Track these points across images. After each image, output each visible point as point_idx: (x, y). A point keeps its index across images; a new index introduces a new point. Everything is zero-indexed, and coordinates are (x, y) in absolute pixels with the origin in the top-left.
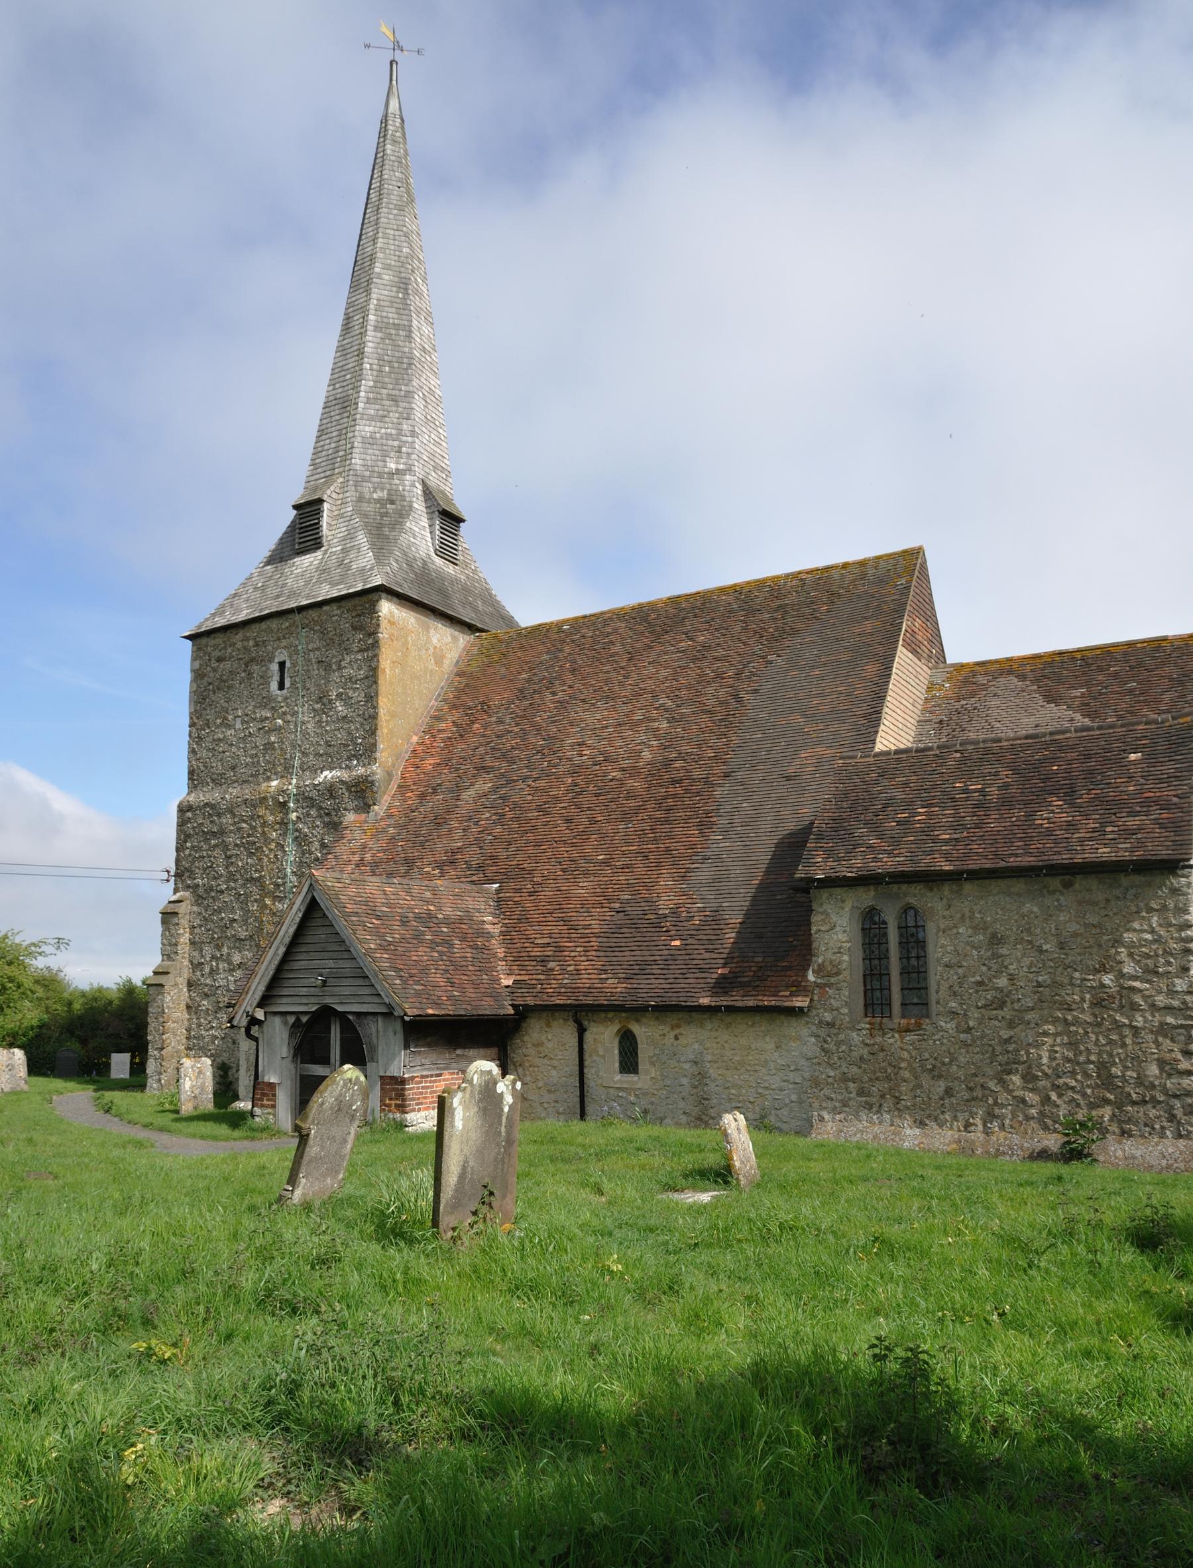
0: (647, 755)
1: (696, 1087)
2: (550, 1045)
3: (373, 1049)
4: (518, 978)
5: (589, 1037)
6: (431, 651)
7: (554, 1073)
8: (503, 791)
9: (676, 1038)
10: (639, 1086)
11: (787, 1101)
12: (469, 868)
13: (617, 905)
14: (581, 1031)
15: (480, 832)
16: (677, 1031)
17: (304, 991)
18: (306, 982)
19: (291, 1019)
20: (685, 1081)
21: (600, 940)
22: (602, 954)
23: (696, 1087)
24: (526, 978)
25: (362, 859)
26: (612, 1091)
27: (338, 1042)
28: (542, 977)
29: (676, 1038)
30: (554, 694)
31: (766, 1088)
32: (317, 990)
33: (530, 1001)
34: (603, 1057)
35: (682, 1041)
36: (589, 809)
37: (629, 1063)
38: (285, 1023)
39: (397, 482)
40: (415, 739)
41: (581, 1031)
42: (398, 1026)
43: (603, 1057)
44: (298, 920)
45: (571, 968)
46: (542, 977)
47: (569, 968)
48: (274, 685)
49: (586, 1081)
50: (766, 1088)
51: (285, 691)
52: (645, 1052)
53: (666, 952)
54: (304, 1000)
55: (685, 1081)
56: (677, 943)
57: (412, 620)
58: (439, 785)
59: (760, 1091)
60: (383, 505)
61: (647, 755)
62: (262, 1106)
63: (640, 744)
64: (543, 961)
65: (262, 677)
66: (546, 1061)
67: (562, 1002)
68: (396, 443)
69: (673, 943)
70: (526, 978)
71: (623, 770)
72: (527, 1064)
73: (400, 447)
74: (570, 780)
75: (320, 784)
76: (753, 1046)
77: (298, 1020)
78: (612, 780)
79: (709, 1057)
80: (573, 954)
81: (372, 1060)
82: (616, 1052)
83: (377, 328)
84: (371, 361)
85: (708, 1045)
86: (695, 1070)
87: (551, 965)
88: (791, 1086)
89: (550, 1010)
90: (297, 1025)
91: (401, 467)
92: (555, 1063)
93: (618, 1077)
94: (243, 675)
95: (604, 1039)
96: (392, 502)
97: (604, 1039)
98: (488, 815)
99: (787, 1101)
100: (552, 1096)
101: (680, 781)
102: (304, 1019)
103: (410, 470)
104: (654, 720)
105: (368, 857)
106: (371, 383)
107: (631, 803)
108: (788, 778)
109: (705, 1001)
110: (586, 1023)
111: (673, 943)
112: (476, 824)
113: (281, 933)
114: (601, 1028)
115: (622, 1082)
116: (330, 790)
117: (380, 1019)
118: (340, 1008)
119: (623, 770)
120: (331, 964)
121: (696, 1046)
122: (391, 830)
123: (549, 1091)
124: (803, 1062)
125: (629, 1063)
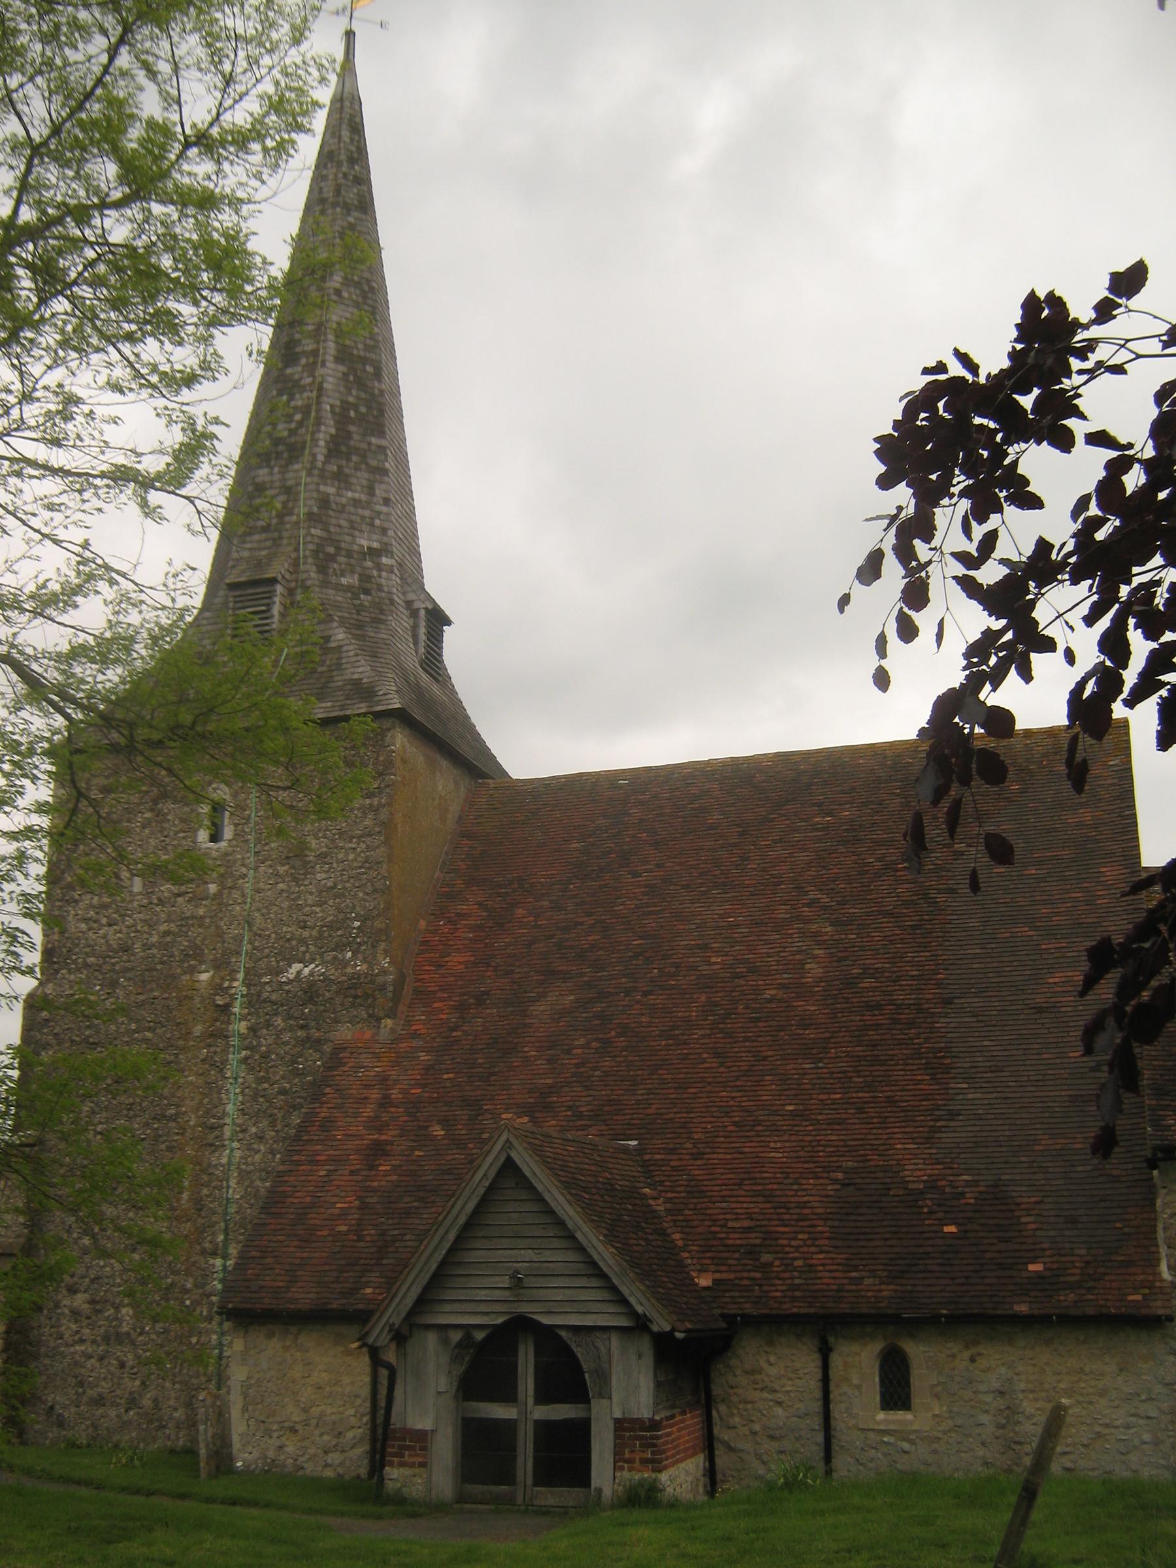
0: (814, 969)
1: (1003, 1427)
2: (773, 1371)
3: (603, 1377)
4: (717, 1276)
5: (836, 1360)
6: (436, 802)
7: (779, 1411)
8: (598, 1008)
9: (973, 1360)
10: (915, 1427)
11: (1136, 1442)
12: (580, 1116)
13: (840, 1176)
14: (825, 1352)
15: (577, 1066)
16: (973, 1351)
17: (482, 1295)
18: (486, 1282)
19: (456, 1337)
20: (985, 1419)
21: (829, 1223)
22: (840, 1243)
23: (1003, 1427)
24: (732, 1276)
25: (386, 1097)
26: (871, 1435)
27: (531, 1370)
28: (758, 1275)
29: (973, 1360)
30: (635, 874)
31: (1107, 1426)
32: (507, 1293)
33: (749, 1309)
34: (859, 1387)
35: (982, 1363)
36: (747, 1039)
37: (896, 1393)
38: (445, 1342)
39: (369, 564)
40: (422, 924)
41: (825, 1352)
42: (645, 1345)
43: (859, 1387)
44: (482, 1191)
45: (799, 1263)
46: (758, 1275)
47: (796, 1263)
48: (203, 835)
49: (833, 1423)
50: (1107, 1426)
51: (223, 844)
52: (921, 1378)
53: (939, 1242)
54: (483, 1308)
55: (985, 1419)
56: (952, 1229)
57: (422, 759)
58: (487, 993)
59: (1098, 1429)
60: (356, 596)
61: (814, 969)
62: (402, 1465)
63: (799, 952)
64: (752, 1252)
65: (183, 821)
66: (765, 1395)
67: (802, 1311)
68: (367, 513)
69: (946, 1229)
70: (732, 1276)
71: (782, 986)
72: (734, 1399)
73: (372, 519)
74: (703, 998)
75: (290, 982)
76: (1087, 1370)
77: (468, 1337)
78: (770, 1001)
79: (1022, 1386)
80: (794, 1243)
81: (601, 1396)
82: (877, 1379)
83: (338, 360)
84: (331, 401)
85: (1021, 1368)
86: (1001, 1403)
87: (766, 1258)
88: (1141, 1422)
89: (776, 1324)
90: (467, 1342)
91: (375, 545)
92: (780, 1397)
93: (881, 1416)
94: (148, 815)
95: (859, 1362)
96: (367, 592)
97: (859, 1362)
98: (582, 1041)
99: (1136, 1442)
100: (775, 1444)
101: (878, 1006)
102: (480, 1336)
103: (387, 551)
104: (809, 921)
105: (395, 1094)
106: (333, 431)
107: (810, 1033)
108: (1040, 1010)
109: (1022, 1308)
110: (831, 1340)
111: (946, 1229)
112: (568, 1052)
113: (455, 1211)
114: (856, 1347)
115: (886, 1421)
116: (310, 991)
117: (615, 1340)
118: (546, 1320)
119: (782, 986)
120: (530, 1255)
121: (1003, 1370)
122: (423, 1057)
123: (772, 1437)
124: (1159, 1388)
125: (896, 1393)
